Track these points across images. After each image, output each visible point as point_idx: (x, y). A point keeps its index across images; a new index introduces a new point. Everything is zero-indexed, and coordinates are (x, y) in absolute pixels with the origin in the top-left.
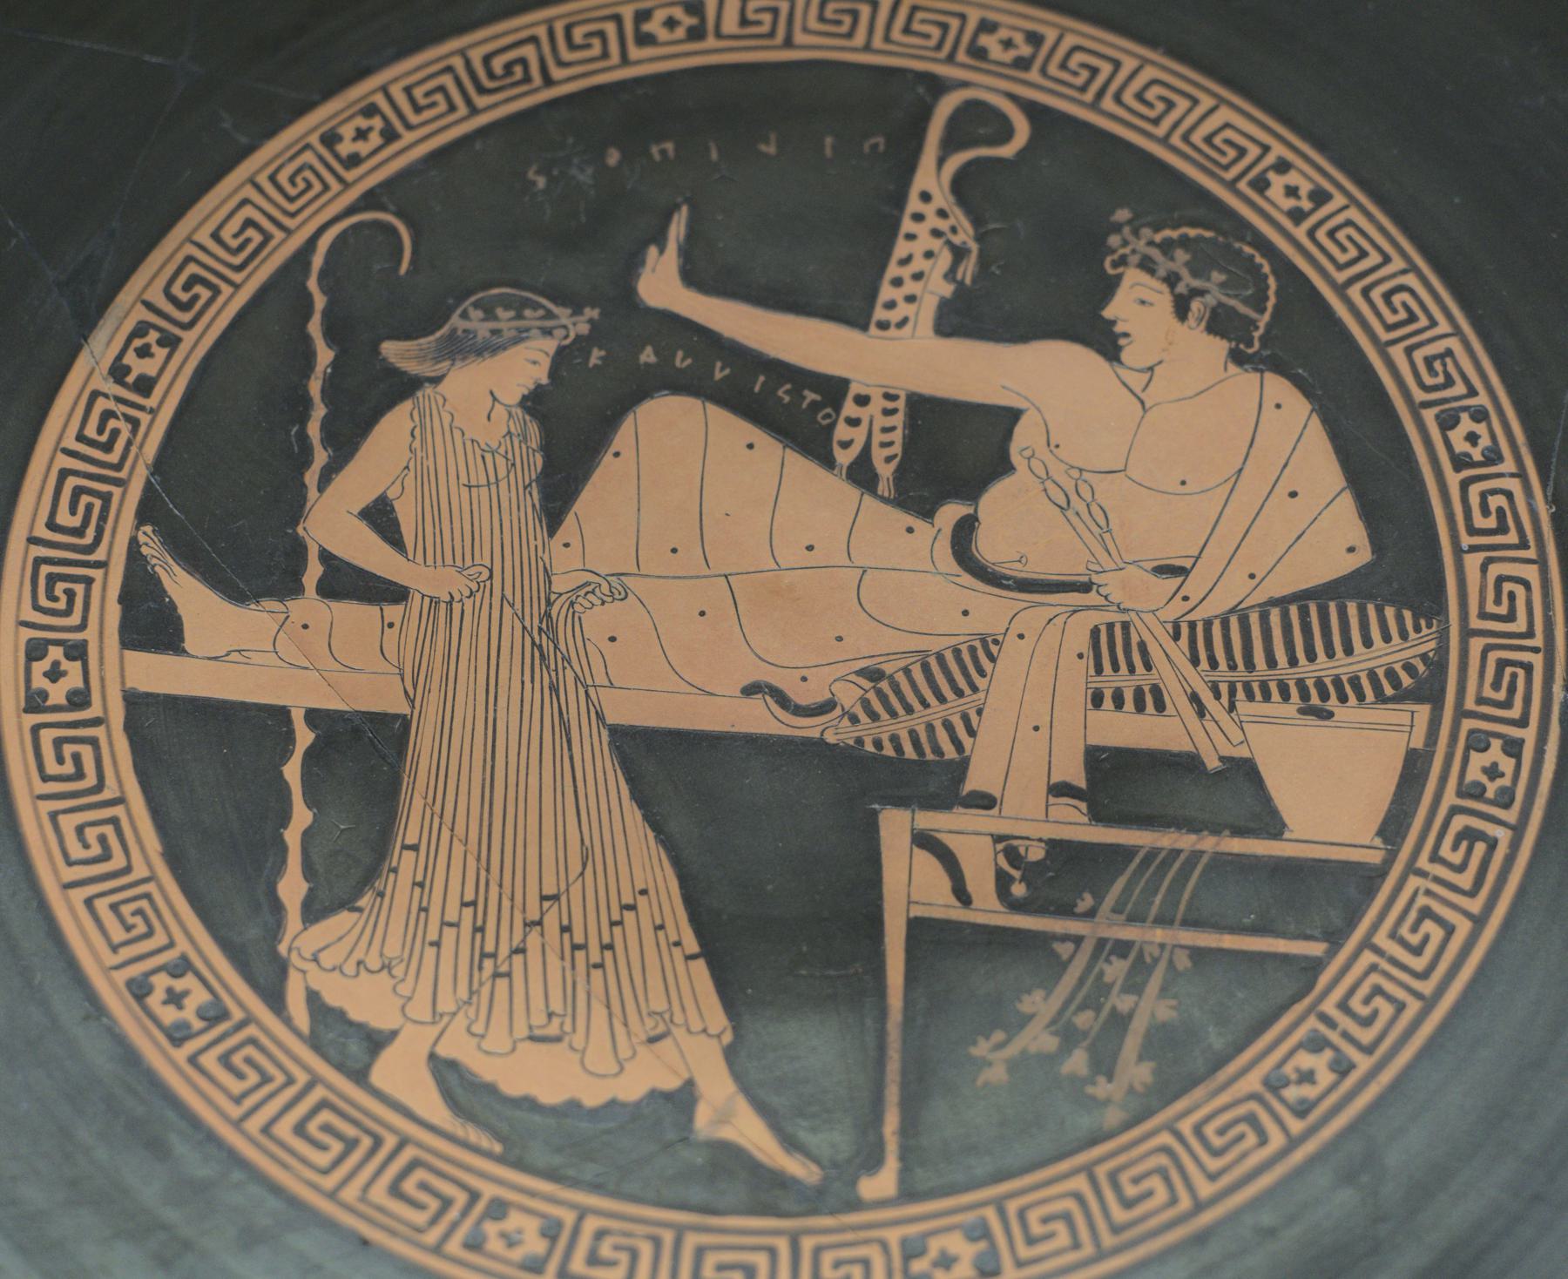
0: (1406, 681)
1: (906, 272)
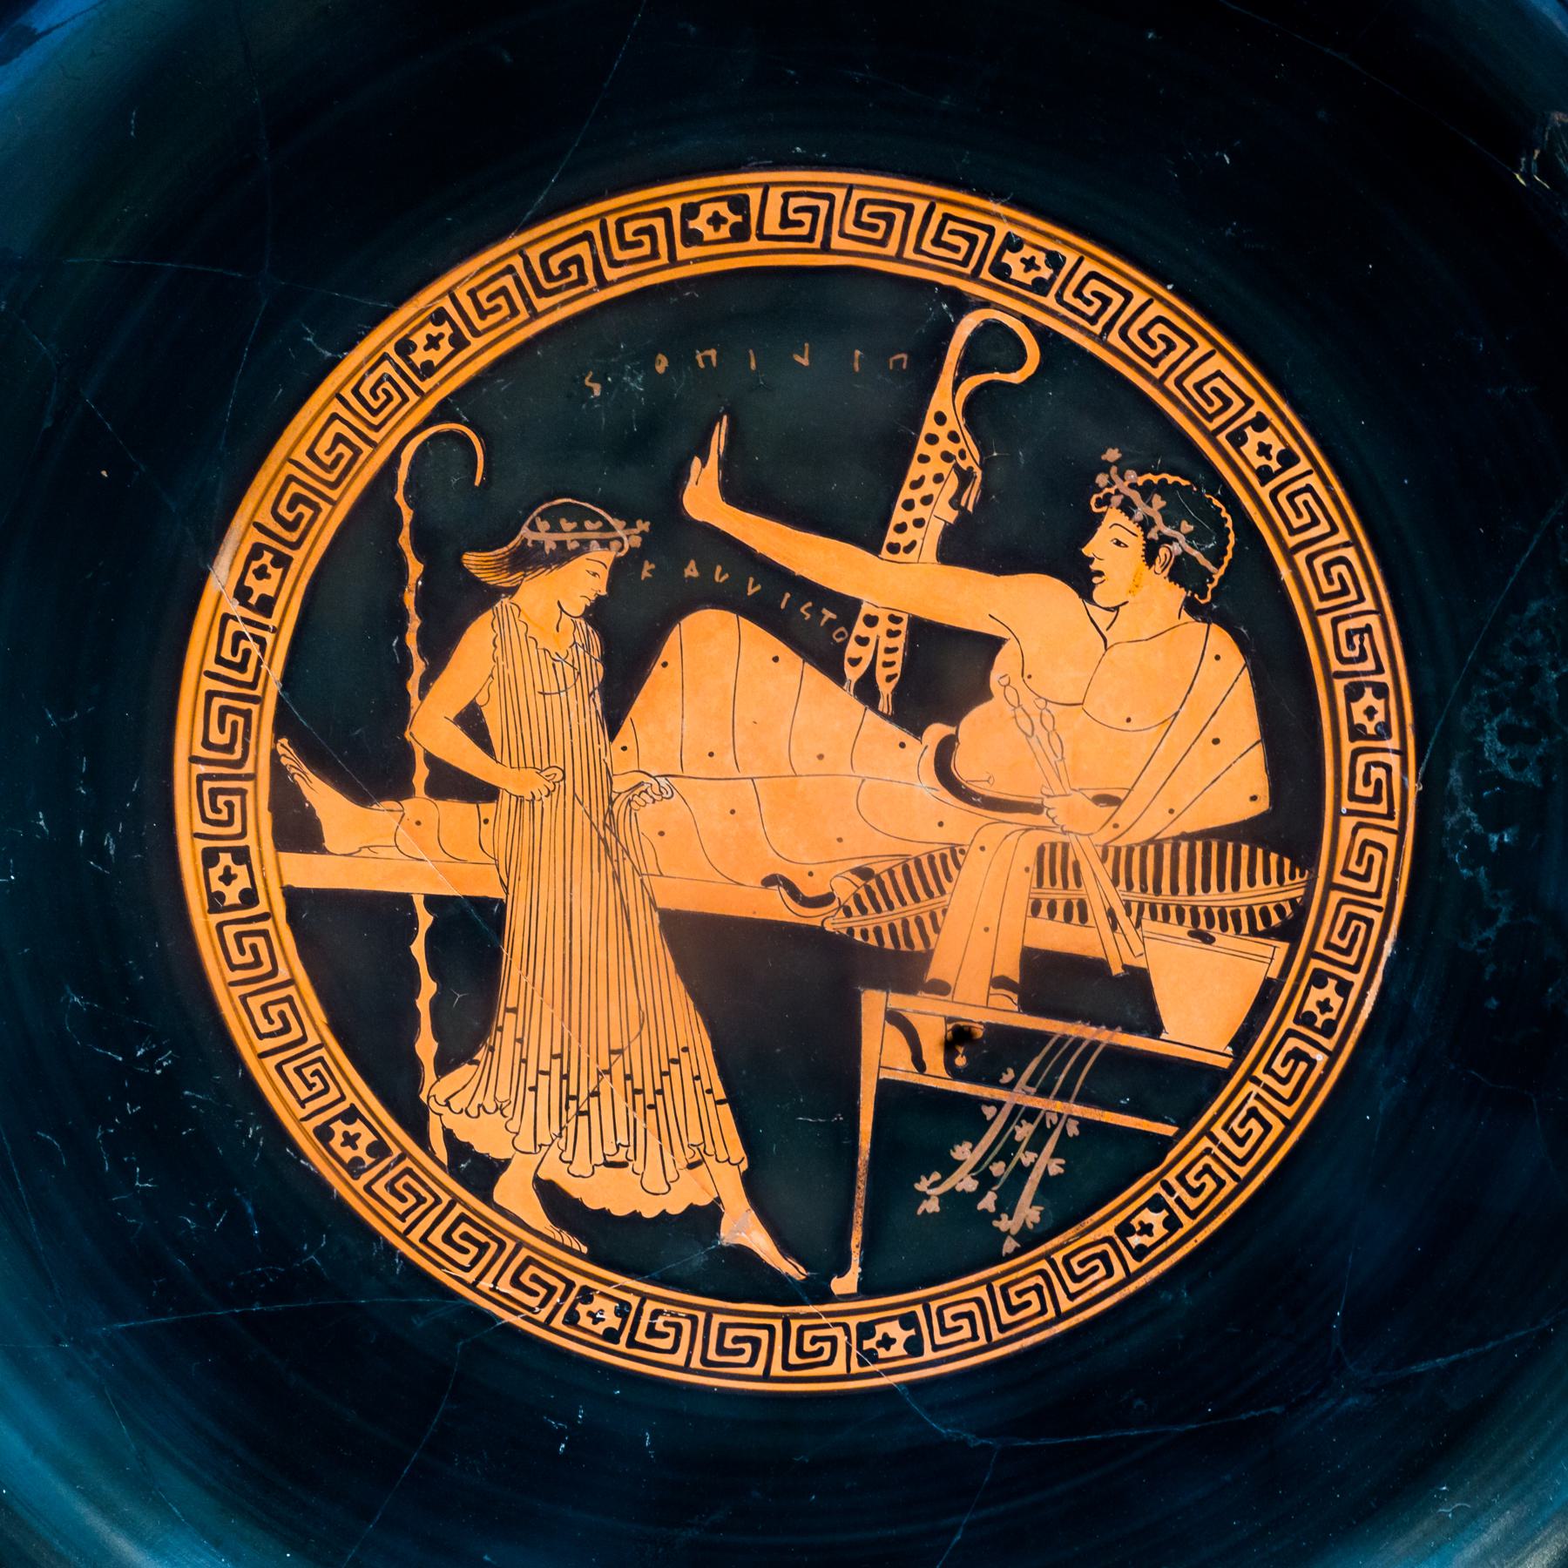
0: (1275, 920)
1: (916, 495)
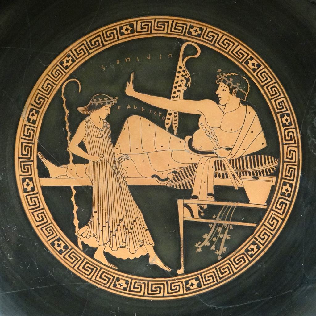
0: (272, 171)
1: (177, 85)
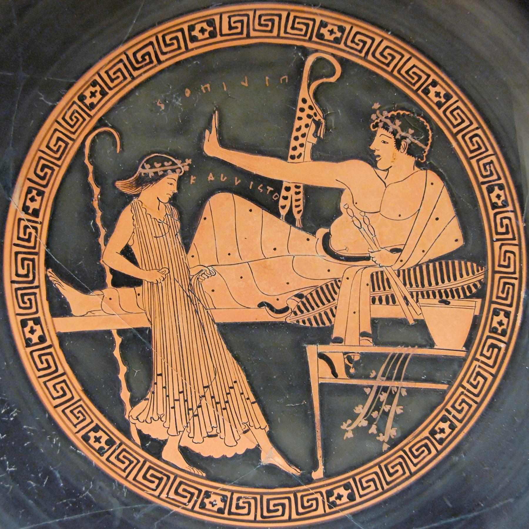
0: (474, 290)
1: (299, 134)
